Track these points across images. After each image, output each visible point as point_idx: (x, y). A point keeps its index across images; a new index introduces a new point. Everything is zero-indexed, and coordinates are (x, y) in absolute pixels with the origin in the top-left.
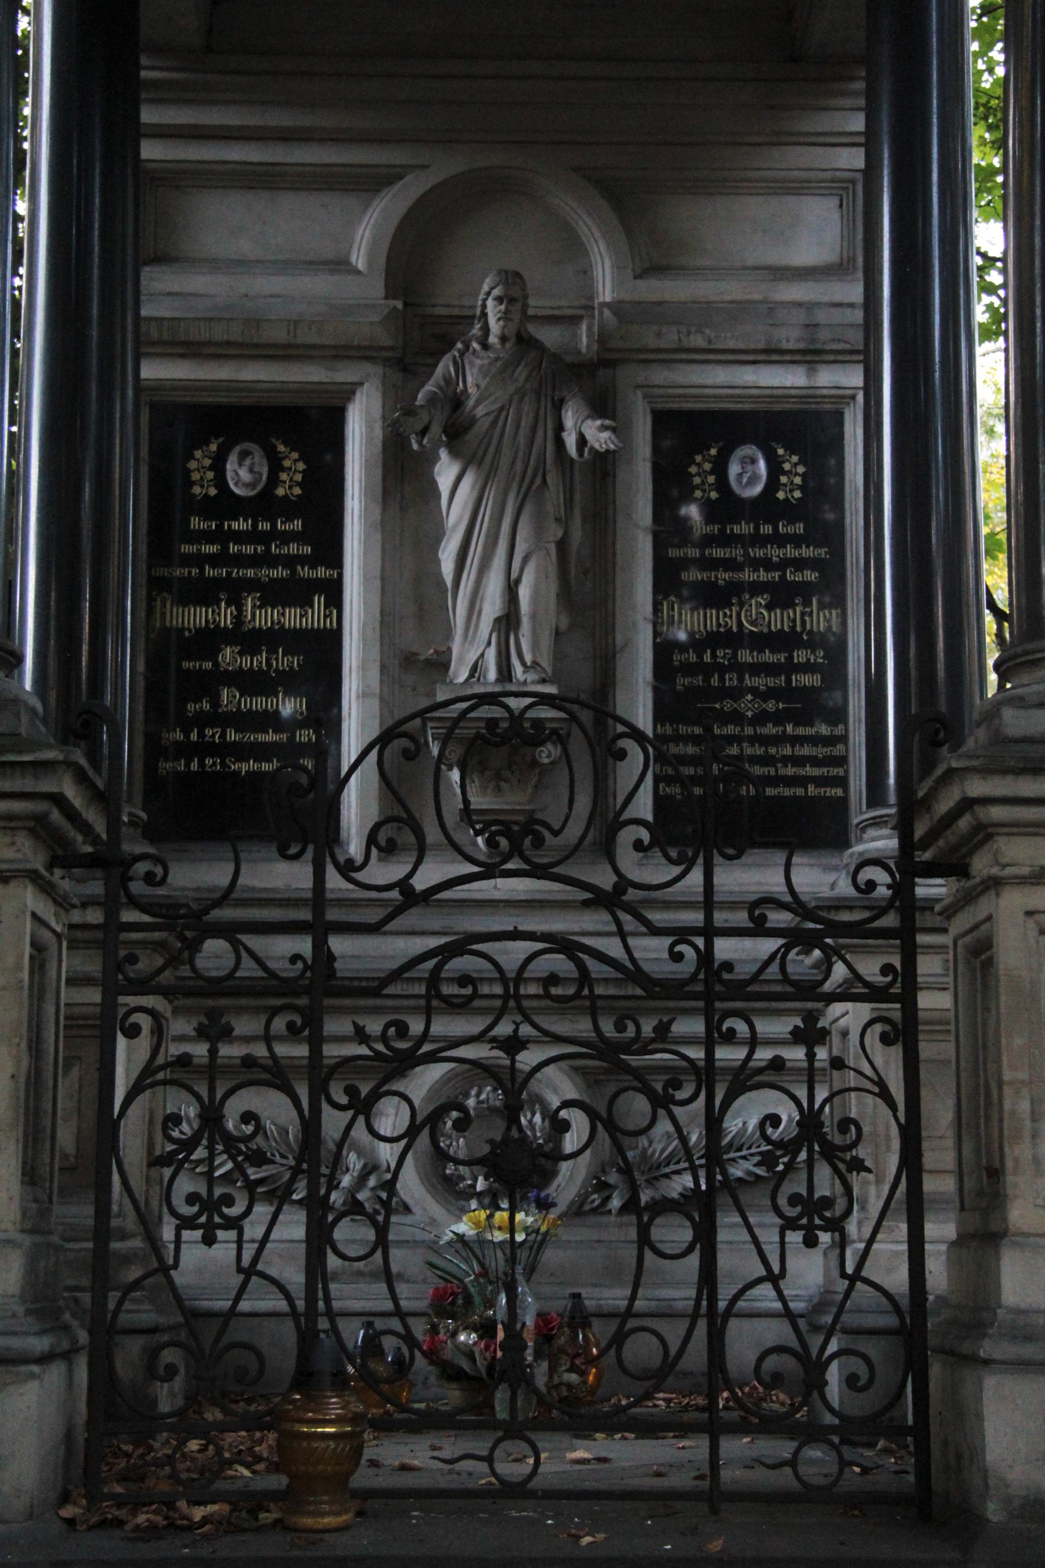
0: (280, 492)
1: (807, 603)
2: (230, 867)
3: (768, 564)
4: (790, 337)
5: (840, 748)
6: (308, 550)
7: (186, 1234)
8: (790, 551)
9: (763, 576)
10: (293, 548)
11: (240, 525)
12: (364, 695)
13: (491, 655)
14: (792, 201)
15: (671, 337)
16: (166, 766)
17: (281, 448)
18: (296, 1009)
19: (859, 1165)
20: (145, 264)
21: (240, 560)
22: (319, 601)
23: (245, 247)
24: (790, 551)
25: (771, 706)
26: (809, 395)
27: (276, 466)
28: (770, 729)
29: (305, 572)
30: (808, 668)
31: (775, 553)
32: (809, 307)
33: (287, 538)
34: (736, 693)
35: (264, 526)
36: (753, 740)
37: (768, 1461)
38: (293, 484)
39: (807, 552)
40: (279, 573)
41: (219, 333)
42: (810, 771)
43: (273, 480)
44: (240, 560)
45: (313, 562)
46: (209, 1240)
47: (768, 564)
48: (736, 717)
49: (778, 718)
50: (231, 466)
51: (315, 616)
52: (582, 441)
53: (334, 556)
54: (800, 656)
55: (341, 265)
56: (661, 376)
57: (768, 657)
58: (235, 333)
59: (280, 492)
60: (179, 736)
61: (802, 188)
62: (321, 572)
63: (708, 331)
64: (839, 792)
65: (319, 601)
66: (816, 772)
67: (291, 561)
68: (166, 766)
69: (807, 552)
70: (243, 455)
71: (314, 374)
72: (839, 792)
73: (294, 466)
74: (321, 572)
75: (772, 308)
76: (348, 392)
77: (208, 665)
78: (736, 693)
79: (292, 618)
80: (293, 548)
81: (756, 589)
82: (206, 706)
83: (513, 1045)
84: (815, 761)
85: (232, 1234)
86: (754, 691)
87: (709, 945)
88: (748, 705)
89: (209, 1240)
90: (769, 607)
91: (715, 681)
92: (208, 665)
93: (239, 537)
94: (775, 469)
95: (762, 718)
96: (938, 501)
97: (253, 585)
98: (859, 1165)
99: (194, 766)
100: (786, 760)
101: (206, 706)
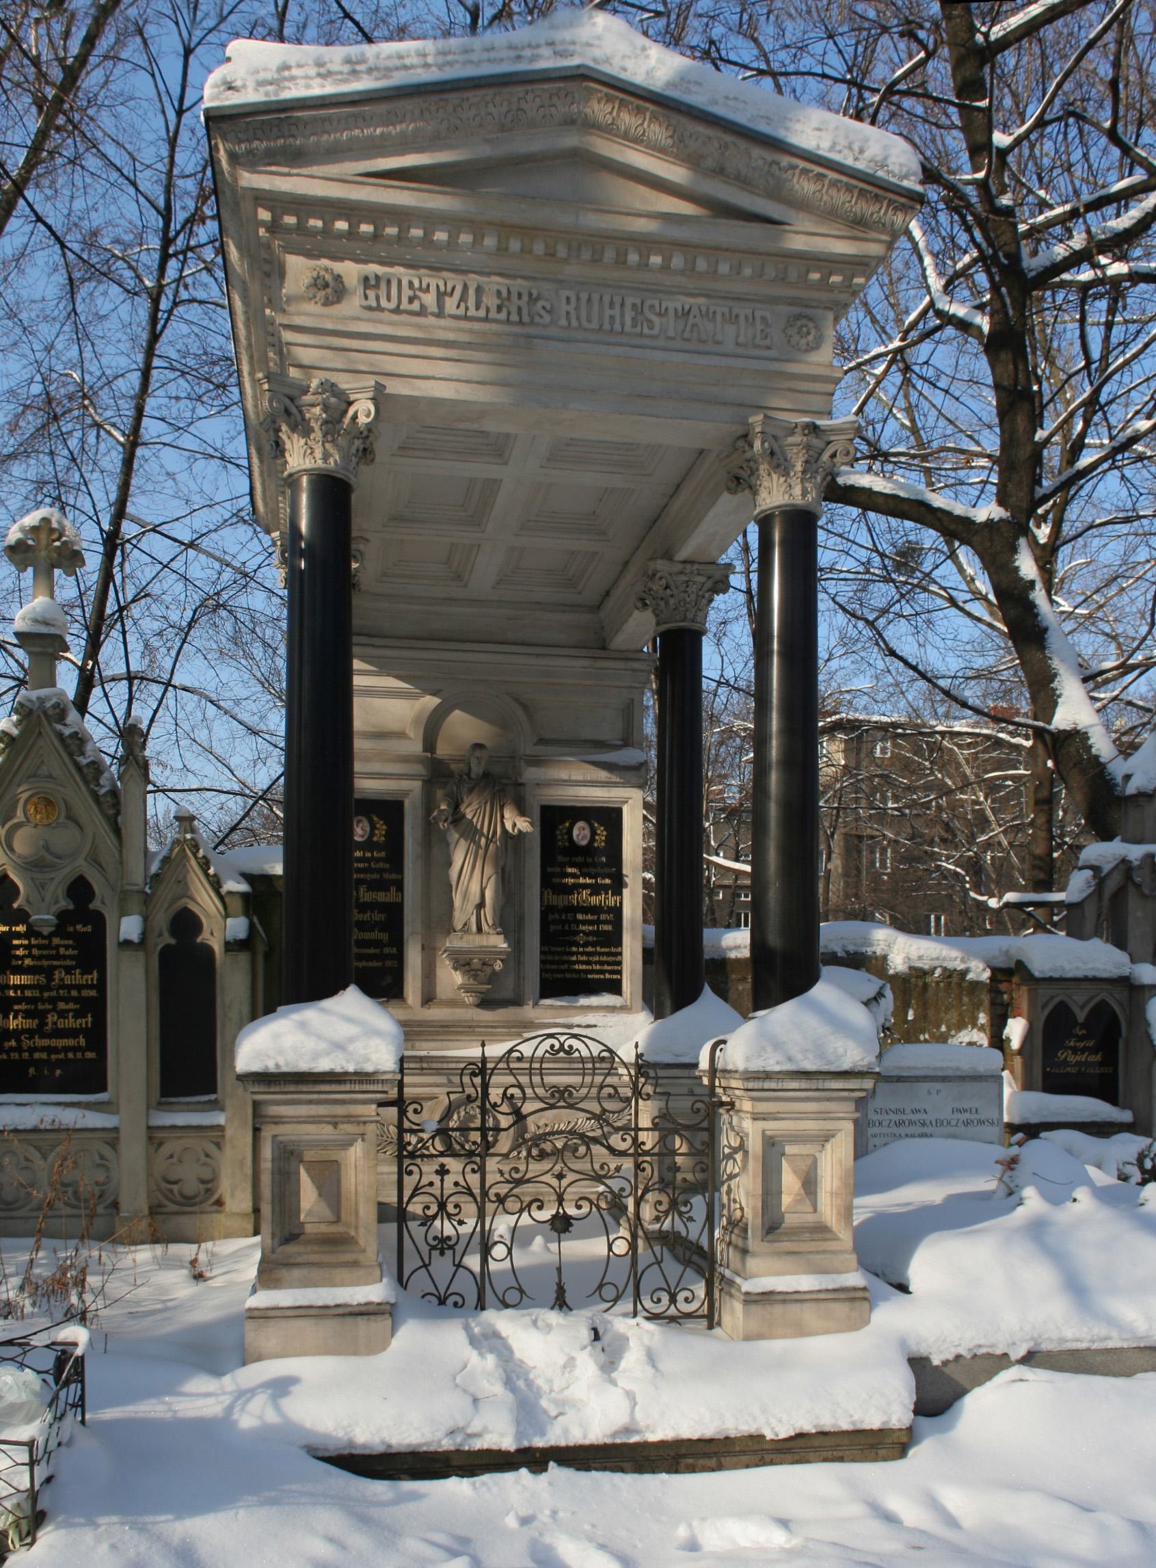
0: (375, 839)
1: (607, 893)
6: (387, 866)
7: (433, 1252)
10: (381, 865)
13: (474, 919)
17: (375, 819)
18: (475, 1163)
19: (691, 1219)
22: (393, 889)
25: (590, 938)
27: (373, 827)
28: (590, 949)
29: (387, 876)
30: (606, 922)
35: (368, 855)
36: (582, 954)
37: (119, 819)
38: (381, 835)
40: (376, 876)
42: (606, 967)
43: (372, 834)
45: (390, 871)
46: (442, 1254)
49: (594, 945)
52: (514, 825)
54: (603, 917)
57: (589, 917)
59: (375, 839)
62: (394, 876)
65: (393, 889)
66: (609, 968)
67: (380, 871)
70: (359, 822)
73: (382, 828)
74: (394, 876)
79: (381, 897)
80: (381, 865)
81: (585, 886)
83: (560, 1176)
84: (609, 964)
85: (451, 1252)
86: (583, 932)
87: (637, 1136)
89: (442, 1254)
90: (591, 895)
91: (567, 927)
94: (594, 833)
95: (586, 944)
98: (691, 1219)
100: (596, 963)
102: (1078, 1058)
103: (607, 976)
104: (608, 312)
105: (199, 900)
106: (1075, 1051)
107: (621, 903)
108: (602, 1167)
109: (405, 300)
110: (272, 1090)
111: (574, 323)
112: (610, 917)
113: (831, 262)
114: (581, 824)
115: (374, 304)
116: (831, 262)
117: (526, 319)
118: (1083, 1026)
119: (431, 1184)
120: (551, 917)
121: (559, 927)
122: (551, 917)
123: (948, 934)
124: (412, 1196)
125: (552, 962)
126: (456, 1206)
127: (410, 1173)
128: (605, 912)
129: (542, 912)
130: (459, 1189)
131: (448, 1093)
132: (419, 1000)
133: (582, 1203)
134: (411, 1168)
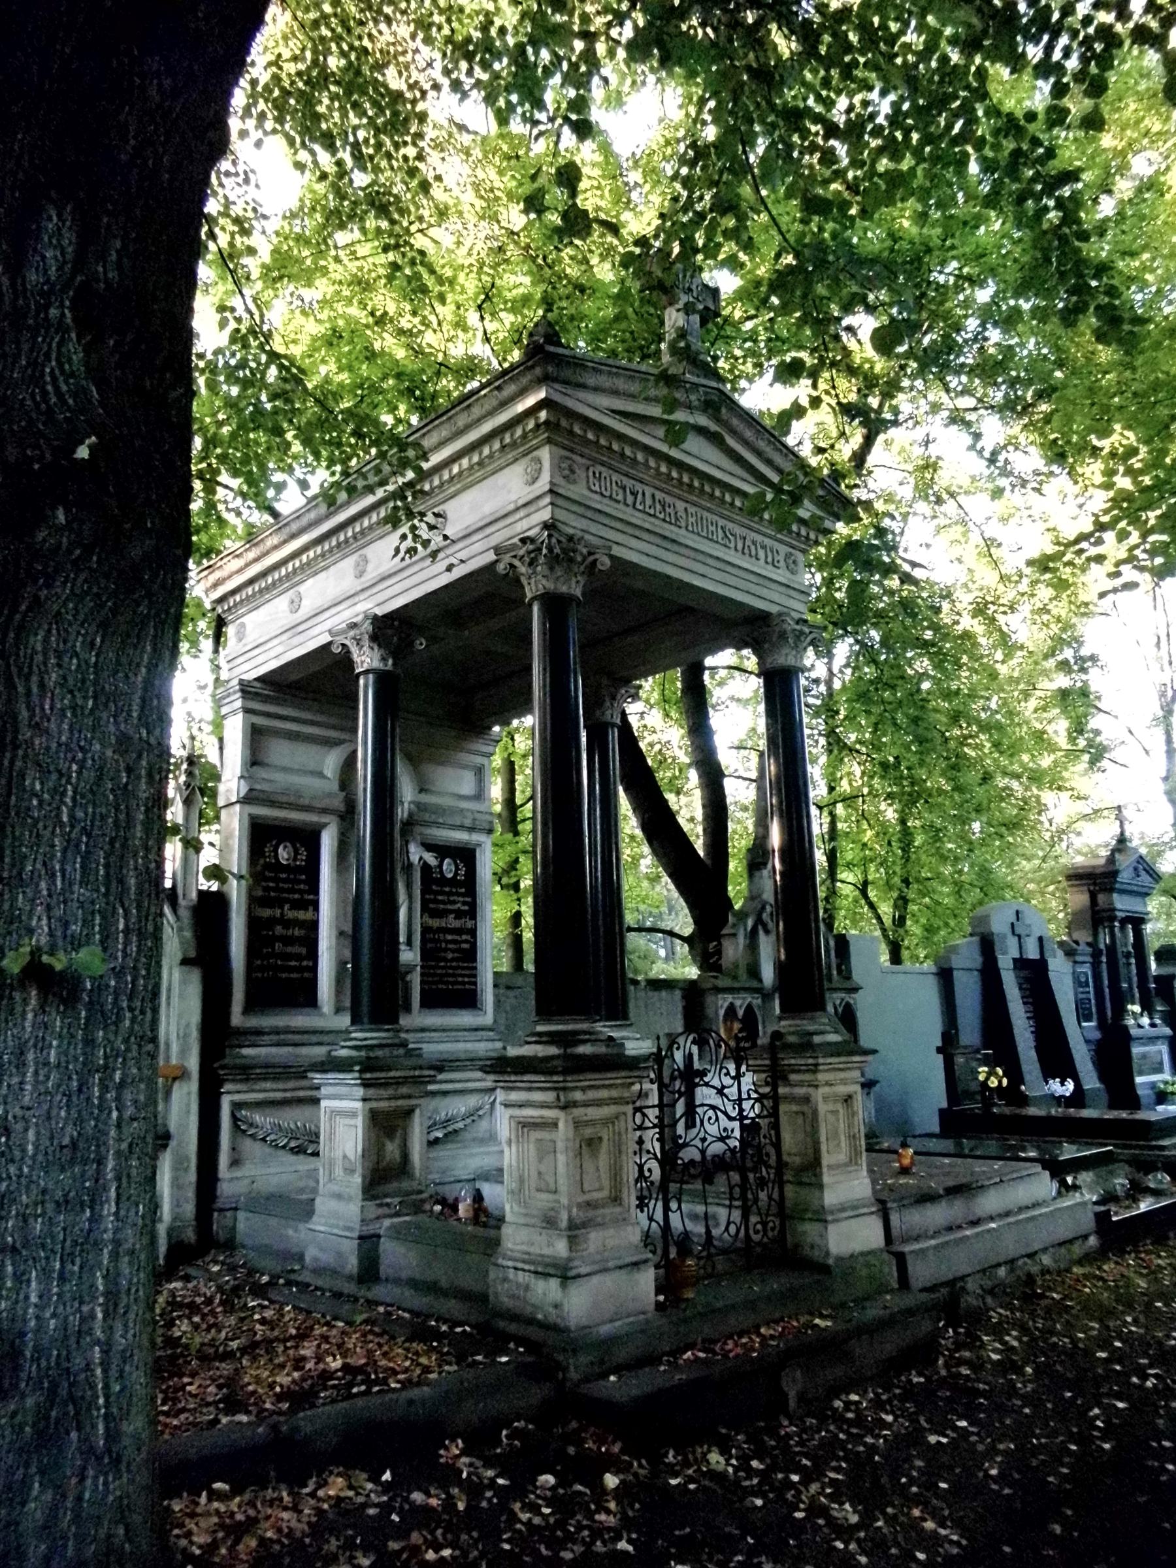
4: (468, 822)
11: (284, 876)
12: (329, 948)
20: (856, 1041)
21: (284, 890)
23: (286, 762)
26: (312, 823)
27: (296, 852)
33: (300, 882)
34: (446, 950)
41: (284, 799)
44: (284, 890)
48: (445, 960)
50: (280, 850)
51: (308, 915)
53: (315, 889)
55: (320, 775)
58: (292, 799)
63: (981, 1077)
67: (301, 892)
71: (313, 818)
73: (303, 853)
76: (325, 825)
78: (446, 950)
79: (301, 915)
88: (450, 956)
93: (285, 881)
96: (596, 928)
97: (287, 901)
112: (468, 937)
132: (333, 1010)
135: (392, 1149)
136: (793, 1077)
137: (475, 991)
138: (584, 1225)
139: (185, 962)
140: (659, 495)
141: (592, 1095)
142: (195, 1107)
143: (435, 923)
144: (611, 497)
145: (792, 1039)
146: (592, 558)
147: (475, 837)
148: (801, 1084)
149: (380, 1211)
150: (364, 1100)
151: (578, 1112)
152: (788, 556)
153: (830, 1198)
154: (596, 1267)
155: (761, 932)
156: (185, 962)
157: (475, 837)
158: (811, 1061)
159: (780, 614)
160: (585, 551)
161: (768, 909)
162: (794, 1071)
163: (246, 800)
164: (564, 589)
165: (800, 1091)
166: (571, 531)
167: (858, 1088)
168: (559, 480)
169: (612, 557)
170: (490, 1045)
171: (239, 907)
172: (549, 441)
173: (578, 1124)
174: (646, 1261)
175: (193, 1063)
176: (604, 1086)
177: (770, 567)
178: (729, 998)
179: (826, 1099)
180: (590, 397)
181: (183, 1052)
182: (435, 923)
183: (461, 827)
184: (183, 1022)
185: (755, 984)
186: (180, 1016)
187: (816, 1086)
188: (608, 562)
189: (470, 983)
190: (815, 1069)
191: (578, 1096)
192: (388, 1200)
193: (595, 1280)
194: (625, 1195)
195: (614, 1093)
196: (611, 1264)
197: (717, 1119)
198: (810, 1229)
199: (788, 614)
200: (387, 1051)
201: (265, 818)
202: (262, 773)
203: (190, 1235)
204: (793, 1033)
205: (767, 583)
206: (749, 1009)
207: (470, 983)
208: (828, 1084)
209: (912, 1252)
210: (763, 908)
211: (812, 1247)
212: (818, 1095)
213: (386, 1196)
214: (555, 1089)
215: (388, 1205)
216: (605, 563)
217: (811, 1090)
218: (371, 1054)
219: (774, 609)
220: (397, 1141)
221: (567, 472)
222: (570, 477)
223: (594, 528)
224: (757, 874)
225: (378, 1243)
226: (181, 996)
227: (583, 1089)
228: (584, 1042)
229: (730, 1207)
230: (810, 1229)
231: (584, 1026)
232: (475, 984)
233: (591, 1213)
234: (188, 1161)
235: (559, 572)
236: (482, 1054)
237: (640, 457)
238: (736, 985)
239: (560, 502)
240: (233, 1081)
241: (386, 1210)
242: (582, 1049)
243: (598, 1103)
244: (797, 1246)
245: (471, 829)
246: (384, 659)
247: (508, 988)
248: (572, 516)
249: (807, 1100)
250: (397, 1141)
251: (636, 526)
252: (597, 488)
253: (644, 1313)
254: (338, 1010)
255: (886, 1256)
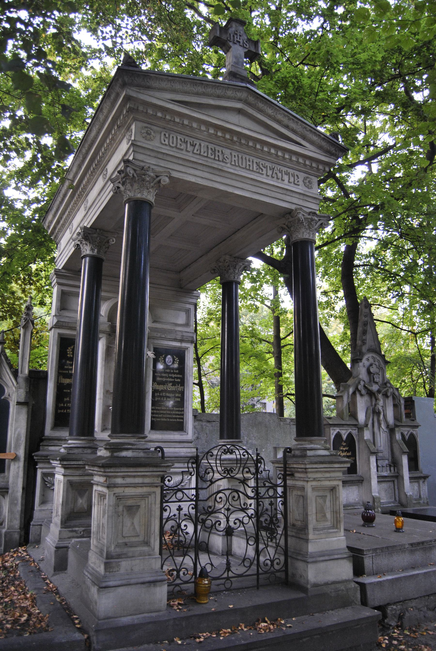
2: (182, 477)
3: (172, 378)
4: (179, 337)
5: (182, 413)
8: (176, 376)
9: (171, 380)
14: (178, 312)
15: (159, 335)
16: (59, 411)
24: (176, 376)
26: (180, 347)
31: (173, 376)
32: (182, 332)
39: (178, 376)
47: (172, 378)
56: (156, 341)
60: (62, 405)
61: (180, 310)
64: (182, 420)
68: (59, 411)
69: (178, 376)
72: (182, 420)
75: (176, 331)
77: (69, 391)
82: (68, 399)
84: (178, 415)
92: (69, 391)
99: (65, 411)
101: (68, 399)
102: (344, 454)
103: (168, 420)
104: (248, 163)
105: (4, 379)
106: (343, 451)
107: (184, 390)
108: (244, 505)
109: (179, 145)
110: (122, 471)
111: (237, 164)
113: (178, 164)
114: (169, 356)
115: (167, 143)
116: (178, 164)
117: (221, 159)
118: (345, 442)
119: (175, 515)
120: (156, 394)
121: (159, 399)
122: (156, 394)
123: (183, 407)
124: (167, 521)
125: (157, 414)
126: (185, 526)
127: (166, 510)
128: (177, 393)
129: (153, 392)
130: (187, 517)
131: (269, 471)
132: (100, 429)
133: (236, 521)
134: (166, 508)
135: (81, 502)
136: (297, 475)
137: (183, 422)
138: (119, 556)
139: (19, 403)
140: (210, 146)
141: (129, 480)
142: (21, 474)
143: (161, 388)
144: (176, 147)
145: (297, 453)
146: (158, 179)
147: (184, 345)
148: (299, 479)
149: (71, 534)
150: (64, 475)
151: (117, 490)
152: (305, 179)
153: (312, 548)
154: (124, 582)
155: (358, 396)
156: (19, 403)
157: (184, 345)
158: (303, 466)
159: (296, 209)
160: (152, 174)
161: (362, 383)
162: (298, 472)
163: (57, 326)
164: (139, 196)
165: (299, 483)
166: (142, 164)
167: (341, 483)
168: (139, 138)
169: (170, 178)
170: (189, 450)
171: (51, 377)
172: (135, 119)
173: (119, 498)
174: (164, 580)
175: (21, 453)
176: (139, 476)
177: (292, 185)
178: (337, 430)
179: (314, 489)
180: (158, 94)
181: (17, 446)
182: (161, 388)
183: (175, 340)
184: (17, 432)
185: (355, 423)
186: (16, 430)
187: (307, 481)
188: (167, 180)
189: (179, 418)
190: (305, 471)
191: (119, 481)
192: (77, 529)
193: (121, 590)
194: (152, 540)
195: (147, 480)
196: (133, 581)
197: (239, 496)
198: (300, 565)
199: (301, 209)
200: (80, 450)
201: (66, 334)
202: (66, 313)
203: (16, 536)
204: (298, 449)
205: (288, 193)
206: (350, 436)
207: (179, 418)
208: (315, 479)
209: (370, 584)
210: (359, 383)
211: (301, 576)
212: (309, 486)
213: (76, 526)
214: (105, 476)
215: (75, 531)
216: (165, 180)
217: (305, 484)
218: (71, 452)
219: (293, 207)
220: (85, 498)
221: (145, 135)
222: (148, 135)
223: (162, 163)
224: (356, 365)
225: (67, 551)
226: (16, 421)
227: (123, 477)
228: (127, 449)
229: (172, 555)
230: (300, 565)
231: (132, 441)
232: (183, 419)
233: (125, 550)
234: (17, 500)
235: (136, 186)
236: (183, 454)
237: (195, 125)
238: (343, 422)
239: (137, 149)
240: (43, 462)
241: (74, 534)
242: (124, 454)
243: (135, 486)
244: (294, 575)
245: (181, 341)
246: (92, 250)
247: (209, 422)
248: (148, 158)
249: (303, 489)
250: (85, 498)
251: (193, 162)
252: (167, 142)
253: (159, 611)
254: (104, 429)
255: (353, 585)
